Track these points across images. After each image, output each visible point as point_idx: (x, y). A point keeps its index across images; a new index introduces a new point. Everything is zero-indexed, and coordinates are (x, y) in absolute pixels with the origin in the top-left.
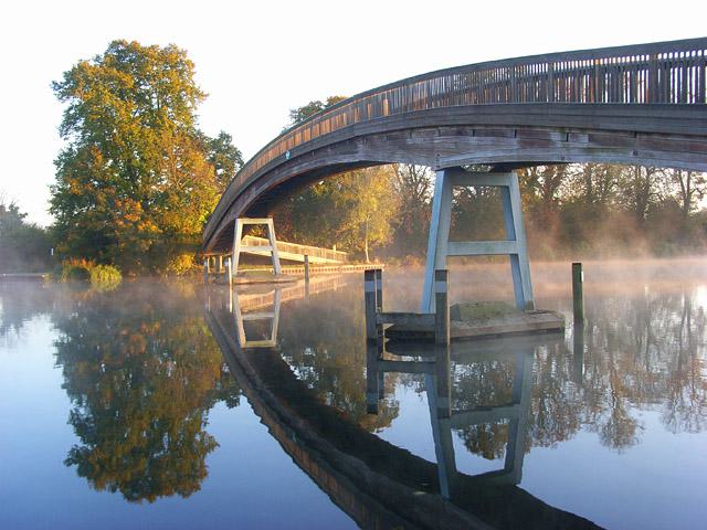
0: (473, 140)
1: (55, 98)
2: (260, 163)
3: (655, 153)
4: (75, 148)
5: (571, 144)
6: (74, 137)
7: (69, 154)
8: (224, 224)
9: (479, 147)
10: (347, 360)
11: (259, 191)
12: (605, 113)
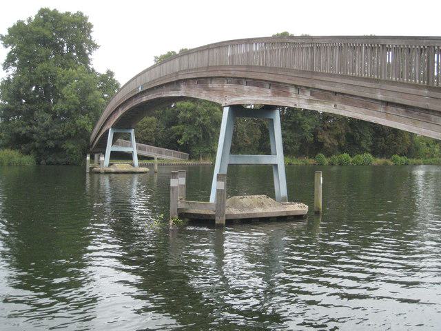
0: (246, 88)
1: (2, 45)
2: (133, 86)
3: (346, 106)
4: (11, 77)
5: (301, 96)
6: (12, 70)
7: (8, 81)
8: (103, 131)
9: (249, 93)
10: (6, 293)
11: (124, 111)
12: (324, 78)
